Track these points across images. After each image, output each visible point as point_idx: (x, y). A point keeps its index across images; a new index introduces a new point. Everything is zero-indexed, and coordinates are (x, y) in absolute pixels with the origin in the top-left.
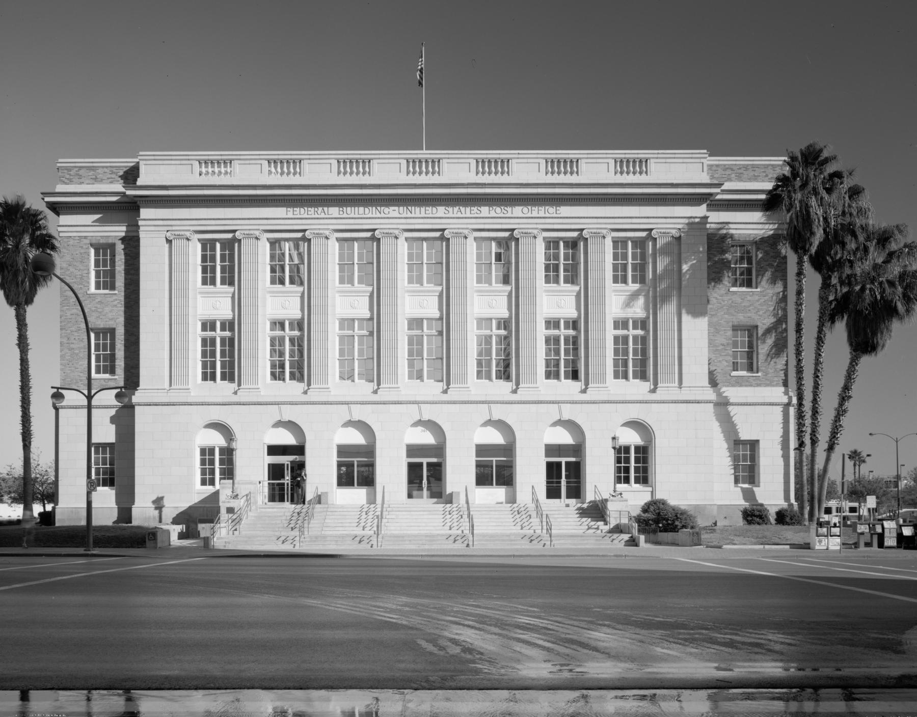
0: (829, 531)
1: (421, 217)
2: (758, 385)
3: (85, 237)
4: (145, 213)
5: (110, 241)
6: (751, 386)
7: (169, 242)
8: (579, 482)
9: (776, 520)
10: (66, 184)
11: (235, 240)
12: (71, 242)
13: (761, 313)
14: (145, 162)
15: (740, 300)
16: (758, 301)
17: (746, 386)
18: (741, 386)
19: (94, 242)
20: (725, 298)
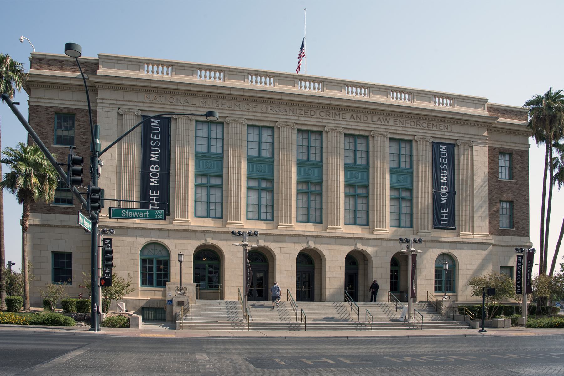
0: (108, 273)
1: (259, 114)
2: (514, 235)
3: (51, 107)
4: (102, 94)
5: (71, 111)
6: (510, 235)
7: (120, 115)
8: (266, 272)
9: (197, 279)
10: (37, 69)
11: (454, 145)
12: (40, 109)
13: (515, 194)
14: (103, 60)
15: (504, 186)
16: (514, 187)
17: (507, 235)
18: (504, 235)
19: (58, 111)
20: (496, 184)
